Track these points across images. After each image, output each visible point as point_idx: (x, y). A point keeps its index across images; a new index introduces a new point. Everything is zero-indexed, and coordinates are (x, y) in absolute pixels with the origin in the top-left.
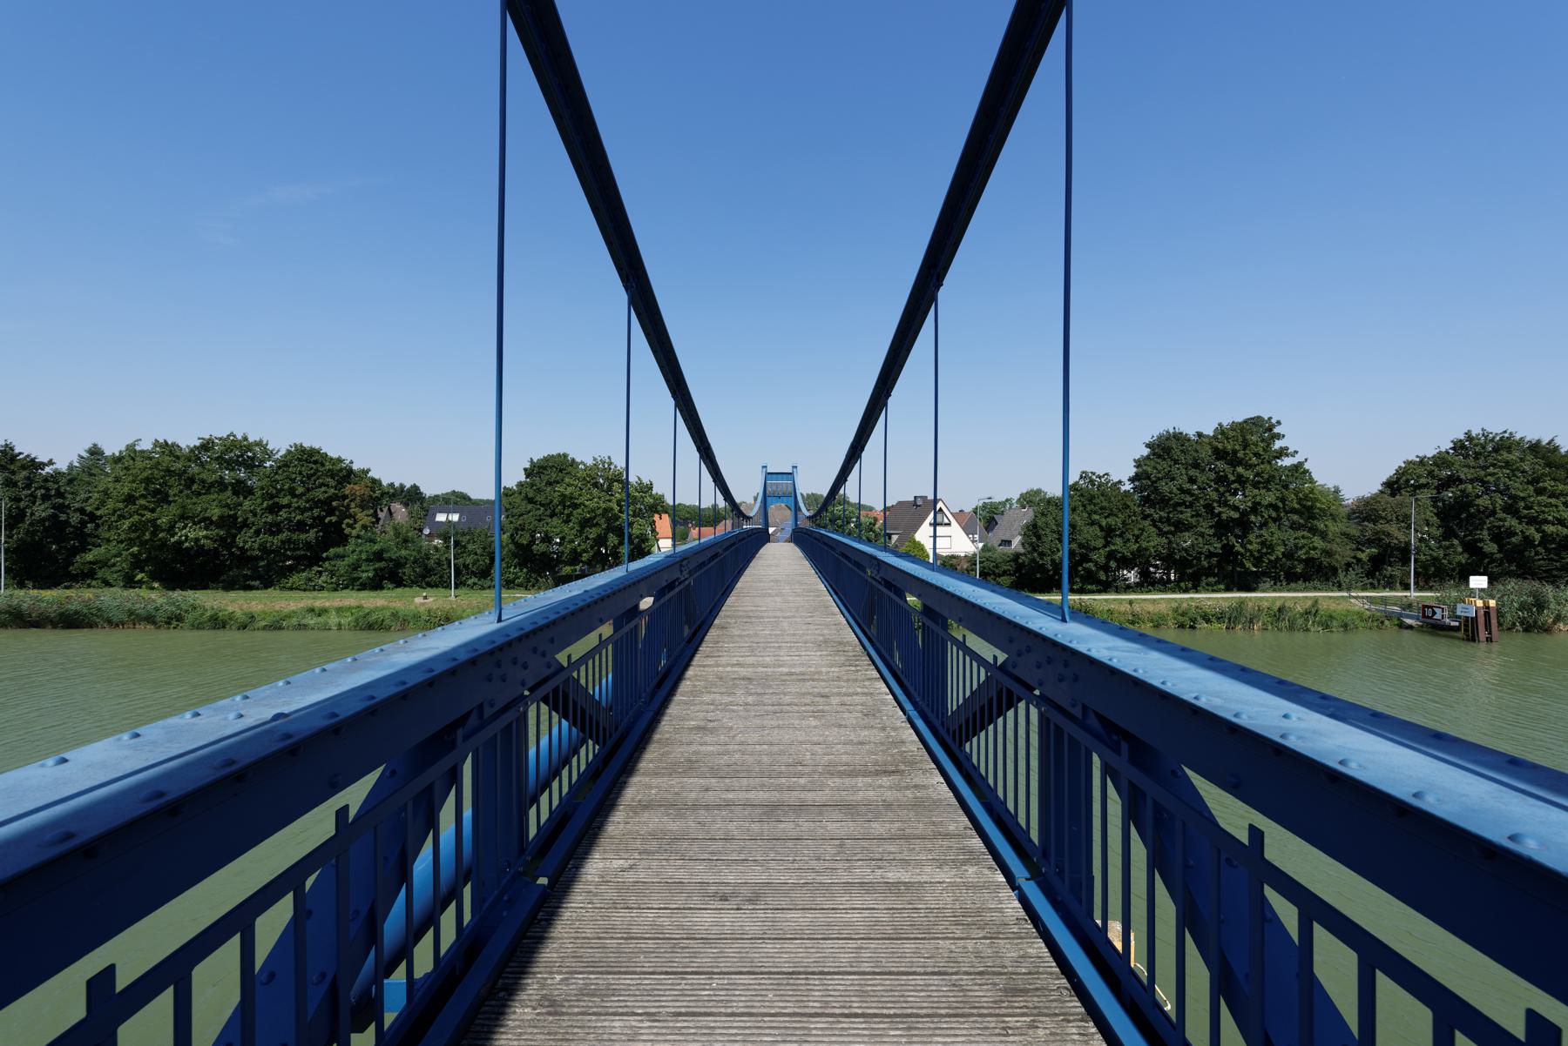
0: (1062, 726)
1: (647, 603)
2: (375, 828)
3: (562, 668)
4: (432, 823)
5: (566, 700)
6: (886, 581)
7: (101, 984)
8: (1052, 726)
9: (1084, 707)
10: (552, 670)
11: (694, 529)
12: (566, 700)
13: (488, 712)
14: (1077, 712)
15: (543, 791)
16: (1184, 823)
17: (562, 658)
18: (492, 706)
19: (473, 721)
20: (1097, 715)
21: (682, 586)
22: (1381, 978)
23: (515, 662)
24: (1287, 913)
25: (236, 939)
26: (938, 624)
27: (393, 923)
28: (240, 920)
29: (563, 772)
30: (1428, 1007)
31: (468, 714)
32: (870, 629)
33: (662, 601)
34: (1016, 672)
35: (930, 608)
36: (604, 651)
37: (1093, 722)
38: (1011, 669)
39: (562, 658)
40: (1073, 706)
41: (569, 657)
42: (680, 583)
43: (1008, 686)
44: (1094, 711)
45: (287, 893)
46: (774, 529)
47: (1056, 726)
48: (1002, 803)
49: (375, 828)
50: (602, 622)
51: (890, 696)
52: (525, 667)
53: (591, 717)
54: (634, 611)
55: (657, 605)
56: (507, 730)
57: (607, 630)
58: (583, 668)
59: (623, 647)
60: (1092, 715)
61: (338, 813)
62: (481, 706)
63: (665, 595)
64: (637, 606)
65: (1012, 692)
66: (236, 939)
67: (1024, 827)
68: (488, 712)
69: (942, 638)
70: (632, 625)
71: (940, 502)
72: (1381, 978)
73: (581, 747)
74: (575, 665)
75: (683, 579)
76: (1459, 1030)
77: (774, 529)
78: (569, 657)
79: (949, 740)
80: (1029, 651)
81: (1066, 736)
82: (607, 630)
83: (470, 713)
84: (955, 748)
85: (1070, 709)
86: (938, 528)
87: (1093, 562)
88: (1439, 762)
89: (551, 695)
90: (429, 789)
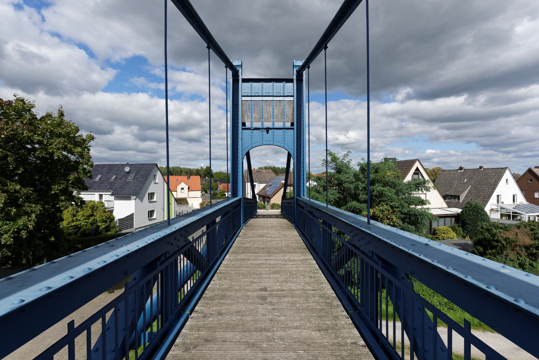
0: (368, 262)
3: (190, 242)
4: (151, 293)
5: (191, 254)
7: (71, 324)
10: (187, 242)
12: (191, 254)
13: (168, 255)
14: (370, 255)
15: (154, 321)
17: (190, 238)
18: (169, 253)
19: (163, 258)
20: (377, 255)
22: (454, 332)
23: (168, 243)
24: (430, 314)
25: (86, 332)
27: (140, 323)
28: (101, 314)
29: (188, 282)
30: (463, 337)
32: (304, 231)
33: (225, 218)
34: (353, 243)
35: (326, 222)
36: (202, 238)
37: (375, 258)
39: (190, 238)
41: (193, 237)
44: (375, 254)
45: (100, 318)
48: (350, 292)
49: (135, 292)
50: (203, 226)
52: (179, 241)
54: (214, 222)
55: (222, 220)
56: (171, 264)
57: (204, 228)
58: (197, 242)
59: (210, 236)
60: (374, 255)
61: (69, 324)
62: (165, 253)
64: (215, 220)
66: (86, 332)
67: (401, 356)
68: (168, 255)
70: (214, 227)
71: (417, 163)
72: (454, 332)
73: (188, 281)
74: (195, 241)
75: (231, 210)
76: (453, 329)
78: (193, 237)
79: (332, 271)
82: (204, 228)
84: (334, 273)
86: (170, 177)
89: (187, 251)
90: (150, 281)
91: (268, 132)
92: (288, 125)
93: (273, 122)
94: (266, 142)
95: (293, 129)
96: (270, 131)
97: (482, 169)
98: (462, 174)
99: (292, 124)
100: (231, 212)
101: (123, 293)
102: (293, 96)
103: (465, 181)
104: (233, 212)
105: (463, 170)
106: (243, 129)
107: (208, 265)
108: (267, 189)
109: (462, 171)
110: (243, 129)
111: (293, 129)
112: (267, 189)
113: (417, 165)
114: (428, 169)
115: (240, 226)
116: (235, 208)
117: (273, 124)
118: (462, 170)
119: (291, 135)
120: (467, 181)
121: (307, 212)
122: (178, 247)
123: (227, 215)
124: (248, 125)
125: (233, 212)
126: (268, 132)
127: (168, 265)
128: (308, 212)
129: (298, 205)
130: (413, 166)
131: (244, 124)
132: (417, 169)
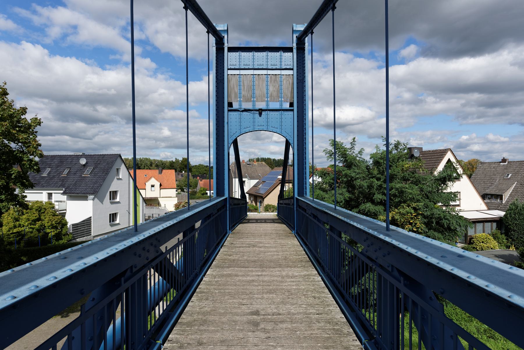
1: (198, 225)
2: (94, 315)
3: (162, 253)
4: (114, 318)
6: (313, 215)
8: (336, 240)
9: (392, 266)
10: (159, 253)
11: (201, 181)
13: (134, 270)
14: (390, 269)
16: (431, 315)
17: (163, 248)
19: (128, 274)
21: (214, 217)
26: (316, 220)
31: (126, 271)
34: (368, 254)
35: (332, 226)
37: (396, 273)
38: (365, 253)
39: (163, 248)
40: (388, 267)
41: (166, 247)
42: (213, 216)
43: (397, 287)
46: (254, 182)
47: (366, 264)
48: (364, 316)
49: (94, 315)
51: (322, 283)
52: (148, 251)
53: (175, 278)
54: (193, 228)
57: (180, 236)
58: (171, 253)
62: (132, 267)
63: (207, 221)
64: (194, 226)
65: (368, 265)
68: (134, 270)
69: (339, 242)
70: (192, 234)
74: (168, 251)
77: (254, 182)
80: (389, 254)
81: (388, 283)
82: (180, 236)
83: (127, 270)
85: (387, 268)
87: (385, 208)
88: (267, 197)
90: (112, 302)
91: (260, 114)
92: (287, 106)
93: (267, 101)
94: (259, 127)
95: (293, 110)
96: (263, 113)
97: (507, 163)
98: (506, 168)
99: (291, 105)
100: (214, 215)
101: (78, 317)
102: (292, 69)
103: (509, 176)
104: (216, 215)
105: (507, 163)
106: (229, 111)
107: (185, 283)
108: (259, 187)
109: (506, 164)
110: (229, 111)
111: (293, 110)
112: (259, 187)
113: (449, 156)
114: (463, 161)
115: (226, 233)
116: (218, 210)
117: (267, 105)
118: (506, 162)
119: (291, 118)
120: (511, 176)
121: (310, 215)
122: (147, 260)
123: (209, 219)
124: (235, 106)
125: (216, 215)
126: (260, 114)
127: (141, 277)
128: (312, 216)
129: (298, 206)
130: (443, 157)
131: (230, 105)
132: (449, 160)
